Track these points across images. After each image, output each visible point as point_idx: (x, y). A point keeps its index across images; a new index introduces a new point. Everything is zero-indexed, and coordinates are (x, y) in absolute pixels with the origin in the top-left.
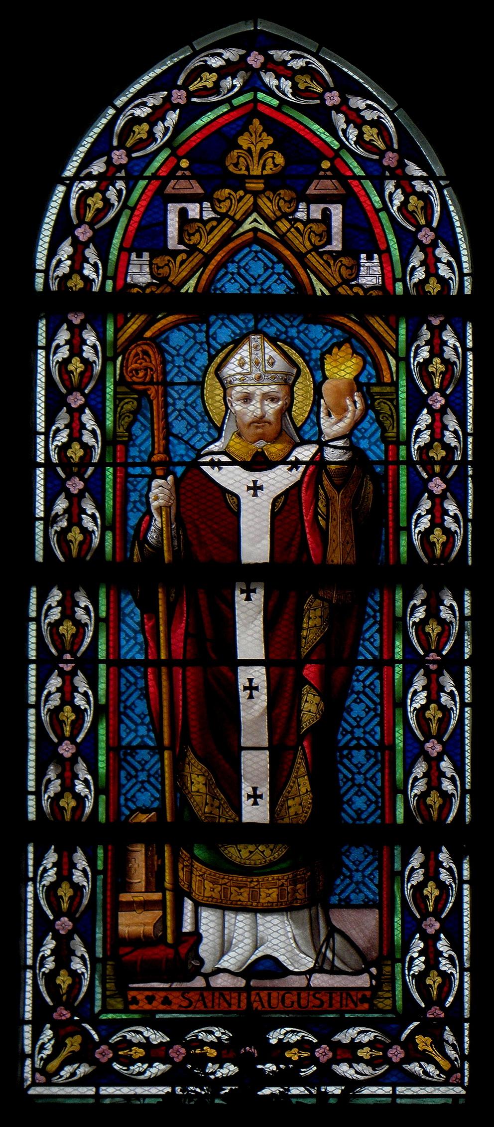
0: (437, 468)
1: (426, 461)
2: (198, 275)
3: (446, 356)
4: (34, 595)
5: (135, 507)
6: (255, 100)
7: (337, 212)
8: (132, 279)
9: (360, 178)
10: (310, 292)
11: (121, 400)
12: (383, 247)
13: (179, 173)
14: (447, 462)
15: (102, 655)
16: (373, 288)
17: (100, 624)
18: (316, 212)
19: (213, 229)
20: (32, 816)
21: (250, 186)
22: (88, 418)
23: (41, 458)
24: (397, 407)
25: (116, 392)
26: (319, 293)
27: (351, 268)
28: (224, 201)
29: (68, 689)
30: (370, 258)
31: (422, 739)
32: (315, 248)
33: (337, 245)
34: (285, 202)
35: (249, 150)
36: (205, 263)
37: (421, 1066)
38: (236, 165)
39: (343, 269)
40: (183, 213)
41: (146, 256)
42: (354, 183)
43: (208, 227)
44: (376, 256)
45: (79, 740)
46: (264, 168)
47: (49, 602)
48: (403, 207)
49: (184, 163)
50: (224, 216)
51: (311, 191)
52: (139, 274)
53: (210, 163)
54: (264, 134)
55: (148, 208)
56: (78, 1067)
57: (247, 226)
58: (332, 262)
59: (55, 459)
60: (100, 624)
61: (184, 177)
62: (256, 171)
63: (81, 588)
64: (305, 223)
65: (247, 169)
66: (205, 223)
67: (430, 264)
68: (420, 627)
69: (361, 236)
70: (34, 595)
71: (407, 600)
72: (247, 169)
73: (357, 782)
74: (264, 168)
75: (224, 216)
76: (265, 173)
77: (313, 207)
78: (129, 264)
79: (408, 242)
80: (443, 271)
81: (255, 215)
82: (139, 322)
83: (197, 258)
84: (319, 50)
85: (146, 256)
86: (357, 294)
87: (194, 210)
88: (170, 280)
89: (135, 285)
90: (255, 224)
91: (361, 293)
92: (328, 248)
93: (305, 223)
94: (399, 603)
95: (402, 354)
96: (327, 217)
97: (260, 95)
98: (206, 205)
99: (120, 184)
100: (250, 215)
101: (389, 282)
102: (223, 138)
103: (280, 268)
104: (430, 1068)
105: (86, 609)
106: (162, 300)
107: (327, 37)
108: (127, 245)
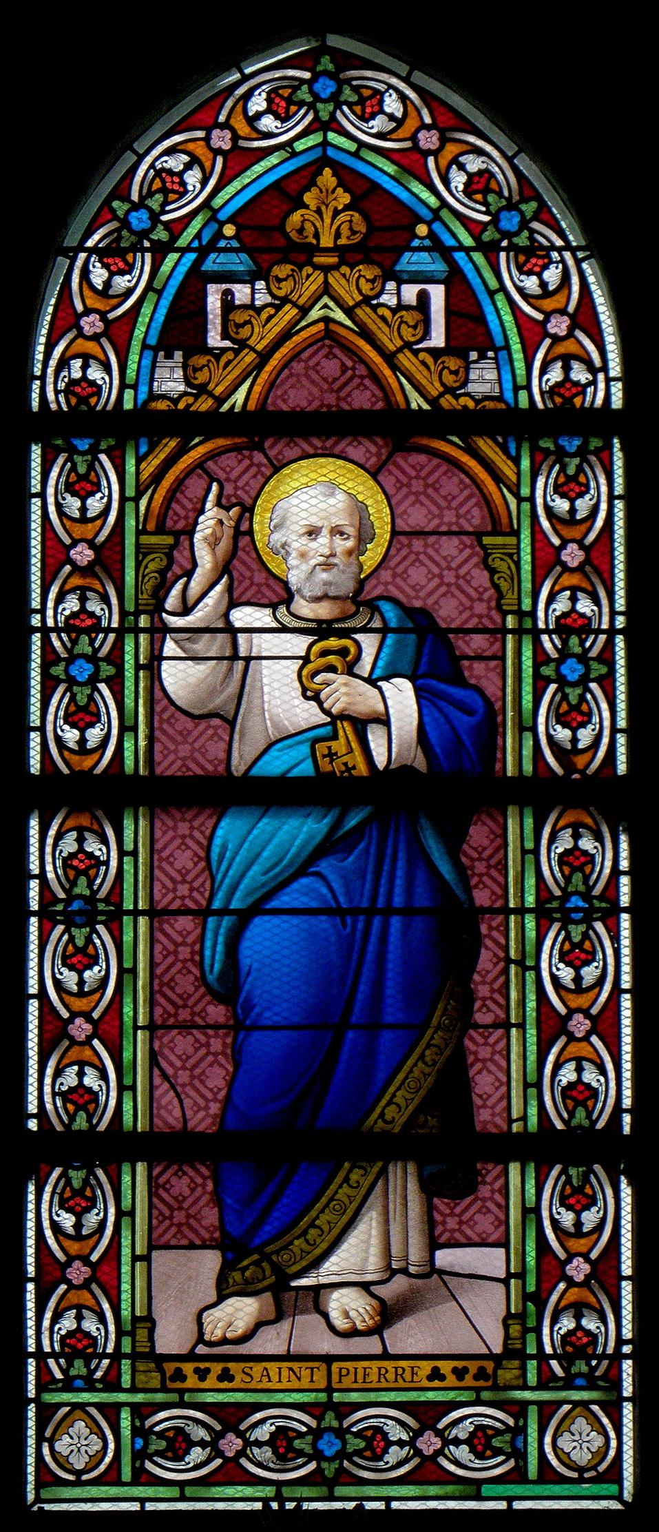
2: (141, 519)
6: (325, 144)
7: (437, 294)
9: (467, 250)
10: (402, 405)
12: (499, 341)
13: (222, 244)
18: (410, 293)
19: (229, 362)
24: (518, 564)
26: (414, 406)
33: (438, 339)
36: (259, 367)
41: (178, 355)
42: (460, 257)
49: (229, 230)
50: (285, 300)
53: (266, 235)
54: (340, 190)
57: (315, 314)
66: (259, 311)
75: (285, 300)
77: (404, 287)
81: (325, 299)
83: (250, 357)
85: (178, 355)
86: (465, 407)
89: (163, 397)
96: (423, 297)
101: (508, 386)
102: (287, 193)
108: (152, 341)
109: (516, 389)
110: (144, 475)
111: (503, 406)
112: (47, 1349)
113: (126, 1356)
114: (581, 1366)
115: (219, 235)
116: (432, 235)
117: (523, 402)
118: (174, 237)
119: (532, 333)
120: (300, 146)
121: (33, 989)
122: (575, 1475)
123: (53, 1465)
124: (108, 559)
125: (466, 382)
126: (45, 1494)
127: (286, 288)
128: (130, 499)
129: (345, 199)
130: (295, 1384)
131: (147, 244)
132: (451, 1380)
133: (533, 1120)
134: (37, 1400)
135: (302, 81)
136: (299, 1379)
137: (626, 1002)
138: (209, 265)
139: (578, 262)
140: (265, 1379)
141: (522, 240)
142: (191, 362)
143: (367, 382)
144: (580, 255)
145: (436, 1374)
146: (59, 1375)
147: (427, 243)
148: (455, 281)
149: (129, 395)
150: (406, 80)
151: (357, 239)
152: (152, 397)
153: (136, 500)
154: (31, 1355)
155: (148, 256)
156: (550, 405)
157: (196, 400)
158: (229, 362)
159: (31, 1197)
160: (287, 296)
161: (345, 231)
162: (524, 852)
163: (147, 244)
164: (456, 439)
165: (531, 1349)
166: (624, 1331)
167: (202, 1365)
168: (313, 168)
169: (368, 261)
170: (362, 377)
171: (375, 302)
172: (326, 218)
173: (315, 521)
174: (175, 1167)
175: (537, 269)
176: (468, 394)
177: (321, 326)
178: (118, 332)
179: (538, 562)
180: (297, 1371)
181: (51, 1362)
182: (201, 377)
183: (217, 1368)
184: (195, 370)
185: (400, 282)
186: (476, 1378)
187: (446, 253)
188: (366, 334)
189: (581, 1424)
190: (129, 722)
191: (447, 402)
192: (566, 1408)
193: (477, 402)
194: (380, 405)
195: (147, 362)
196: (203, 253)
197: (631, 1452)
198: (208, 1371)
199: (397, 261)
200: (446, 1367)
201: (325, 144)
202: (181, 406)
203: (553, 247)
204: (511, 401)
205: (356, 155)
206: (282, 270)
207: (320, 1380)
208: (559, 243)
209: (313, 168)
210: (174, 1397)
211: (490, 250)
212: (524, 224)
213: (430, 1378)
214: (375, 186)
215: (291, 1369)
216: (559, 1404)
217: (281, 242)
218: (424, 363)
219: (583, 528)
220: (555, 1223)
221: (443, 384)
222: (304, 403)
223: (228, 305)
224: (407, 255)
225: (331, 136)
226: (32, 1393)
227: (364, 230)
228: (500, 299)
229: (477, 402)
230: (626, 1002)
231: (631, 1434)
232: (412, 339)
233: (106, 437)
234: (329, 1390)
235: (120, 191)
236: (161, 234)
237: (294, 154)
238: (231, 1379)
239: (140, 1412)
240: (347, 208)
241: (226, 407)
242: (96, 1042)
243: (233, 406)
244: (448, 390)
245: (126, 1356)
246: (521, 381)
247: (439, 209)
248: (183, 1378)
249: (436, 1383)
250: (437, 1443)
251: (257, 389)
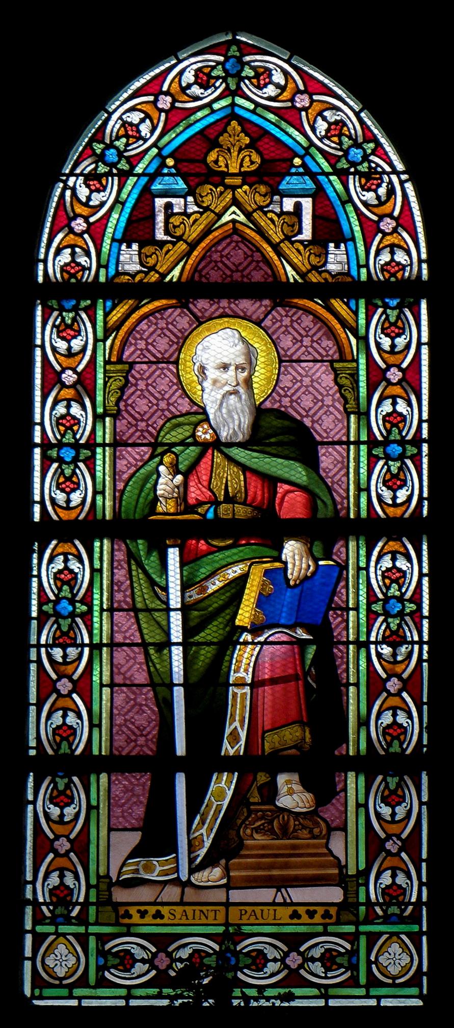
4: (31, 779)
6: (233, 105)
7: (307, 204)
8: (123, 268)
9: (327, 175)
10: (284, 279)
11: (110, 378)
13: (165, 171)
17: (95, 574)
19: (168, 251)
20: (40, 279)
21: (228, 181)
24: (357, 382)
26: (292, 280)
27: (319, 256)
33: (307, 234)
36: (188, 254)
39: (312, 257)
40: (169, 206)
41: (135, 246)
42: (322, 178)
44: (342, 245)
46: (241, 166)
53: (194, 165)
54: (242, 135)
55: (138, 200)
57: (226, 218)
60: (95, 574)
62: (234, 169)
65: (227, 166)
69: (328, 230)
70: (31, 779)
72: (227, 166)
76: (242, 170)
81: (233, 208)
82: (126, 307)
83: (182, 247)
85: (135, 246)
86: (325, 279)
89: (126, 274)
90: (234, 216)
91: (330, 280)
92: (300, 237)
93: (279, 216)
95: (362, 331)
96: (298, 206)
98: (190, 199)
102: (209, 138)
108: (119, 236)
109: (359, 267)
111: (349, 279)
112: (41, 900)
113: (93, 904)
114: (394, 910)
115: (163, 165)
116: (304, 165)
117: (364, 276)
118: (133, 167)
119: (370, 229)
120: (216, 106)
121: (37, 498)
122: (390, 981)
123: (44, 975)
124: (85, 383)
129: (247, 140)
130: (204, 921)
131: (115, 171)
132: (305, 919)
133: (363, 746)
134: (33, 932)
135: (218, 63)
136: (207, 918)
138: (156, 186)
139: (402, 183)
141: (364, 168)
142: (143, 251)
143: (261, 264)
144: (404, 177)
145: (295, 915)
146: (48, 914)
147: (301, 170)
148: (318, 195)
149: (103, 271)
150: (288, 61)
151: (253, 167)
152: (118, 274)
153: (104, 341)
155: (116, 179)
156: (382, 278)
159: (35, 561)
160: (208, 206)
162: (359, 569)
163: (115, 171)
165: (362, 899)
168: (226, 120)
169: (261, 182)
170: (258, 262)
172: (235, 159)
173: (226, 360)
174: (124, 753)
175: (374, 187)
178: (96, 231)
179: (370, 382)
180: (206, 912)
181: (44, 908)
182: (151, 261)
183: (152, 910)
185: (283, 195)
186: (323, 917)
187: (313, 176)
188: (260, 231)
189: (395, 948)
190: (99, 487)
191: (314, 278)
192: (385, 937)
193: (333, 276)
194: (271, 279)
195: (115, 250)
196: (152, 177)
199: (279, 183)
201: (233, 105)
202: (138, 278)
203: (384, 172)
204: (356, 278)
207: (221, 918)
208: (388, 169)
209: (226, 120)
210: (124, 930)
211: (343, 175)
212: (366, 158)
213: (291, 917)
214: (267, 133)
215: (201, 911)
216: (381, 934)
217: (203, 170)
218: (298, 250)
219: (401, 356)
220: (378, 815)
224: (288, 178)
225: (239, 101)
226: (28, 926)
227: (259, 162)
228: (349, 208)
233: (85, 299)
235: (99, 136)
236: (124, 165)
237: (213, 112)
239: (102, 939)
240: (247, 146)
241: (168, 279)
242: (75, 696)
243: (172, 278)
244: (314, 268)
245: (93, 904)
246: (362, 262)
247: (309, 147)
248: (130, 917)
249: (295, 921)
250: (300, 960)
251: (188, 267)
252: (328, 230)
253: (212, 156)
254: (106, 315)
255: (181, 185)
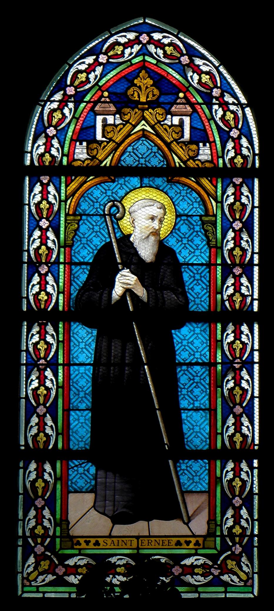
0: (237, 539)
1: (231, 535)
2: (112, 155)
3: (243, 431)
5: (76, 370)
6: (144, 61)
7: (187, 120)
9: (200, 104)
10: (173, 165)
12: (211, 140)
13: (103, 99)
14: (242, 535)
15: (61, 361)
16: (207, 161)
18: (176, 120)
19: (121, 129)
20: (25, 309)
22: (46, 512)
23: (20, 533)
25: (66, 220)
26: (177, 165)
28: (127, 115)
29: (42, 424)
30: (205, 145)
31: (232, 220)
32: (175, 140)
34: (159, 114)
35: (140, 87)
36: (115, 149)
37: (229, 577)
38: (132, 95)
41: (85, 144)
43: (118, 129)
44: (208, 144)
45: (45, 544)
46: (147, 97)
47: (34, 192)
48: (223, 118)
49: (106, 94)
50: (127, 122)
51: (173, 109)
52: (81, 152)
56: (46, 577)
57: (138, 128)
58: (184, 148)
59: (28, 534)
61: (105, 102)
63: (47, 462)
64: (170, 127)
65: (139, 97)
66: (116, 126)
67: (238, 148)
68: (231, 345)
69: (200, 136)
71: (224, 330)
72: (139, 97)
73: (196, 278)
74: (147, 97)
75: (127, 122)
77: (174, 118)
78: (75, 148)
79: (225, 137)
80: (245, 152)
81: (143, 122)
83: (111, 145)
84: (178, 34)
85: (85, 144)
87: (110, 119)
88: (97, 157)
90: (144, 127)
92: (182, 140)
94: (219, 332)
96: (182, 122)
97: (147, 58)
99: (71, 105)
100: (141, 121)
101: (215, 158)
102: (129, 79)
103: (155, 149)
104: (235, 578)
105: (51, 427)
106: (93, 170)
107: (182, 26)
110: (68, 192)
115: (102, 96)
117: (221, 165)
125: (198, 154)
126: (26, 589)
127: (127, 118)
128: (63, 201)
136: (126, 545)
137: (256, 401)
140: (112, 544)
145: (178, 543)
151: (154, 98)
153: (66, 201)
154: (20, 537)
157: (124, 126)
158: (121, 129)
161: (150, 96)
164: (193, 179)
166: (255, 249)
167: (88, 539)
171: (162, 123)
172: (144, 89)
176: (199, 160)
177: (141, 133)
184: (92, 150)
186: (195, 545)
187: (192, 105)
188: (158, 135)
191: (191, 164)
193: (202, 163)
196: (95, 103)
197: (257, 236)
198: (90, 541)
200: (182, 540)
201: (144, 61)
205: (156, 65)
206: (127, 110)
207: (135, 545)
213: (176, 545)
221: (189, 155)
222: (132, 163)
223: (105, 125)
229: (202, 163)
230: (256, 401)
231: (257, 233)
232: (177, 138)
234: (138, 549)
238: (99, 545)
243: (106, 163)
245: (58, 537)
248: (80, 544)
252: (200, 136)
253: (130, 92)
254: (67, 186)
255: (113, 108)
